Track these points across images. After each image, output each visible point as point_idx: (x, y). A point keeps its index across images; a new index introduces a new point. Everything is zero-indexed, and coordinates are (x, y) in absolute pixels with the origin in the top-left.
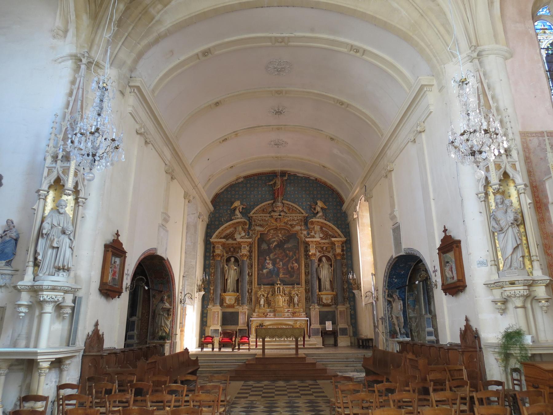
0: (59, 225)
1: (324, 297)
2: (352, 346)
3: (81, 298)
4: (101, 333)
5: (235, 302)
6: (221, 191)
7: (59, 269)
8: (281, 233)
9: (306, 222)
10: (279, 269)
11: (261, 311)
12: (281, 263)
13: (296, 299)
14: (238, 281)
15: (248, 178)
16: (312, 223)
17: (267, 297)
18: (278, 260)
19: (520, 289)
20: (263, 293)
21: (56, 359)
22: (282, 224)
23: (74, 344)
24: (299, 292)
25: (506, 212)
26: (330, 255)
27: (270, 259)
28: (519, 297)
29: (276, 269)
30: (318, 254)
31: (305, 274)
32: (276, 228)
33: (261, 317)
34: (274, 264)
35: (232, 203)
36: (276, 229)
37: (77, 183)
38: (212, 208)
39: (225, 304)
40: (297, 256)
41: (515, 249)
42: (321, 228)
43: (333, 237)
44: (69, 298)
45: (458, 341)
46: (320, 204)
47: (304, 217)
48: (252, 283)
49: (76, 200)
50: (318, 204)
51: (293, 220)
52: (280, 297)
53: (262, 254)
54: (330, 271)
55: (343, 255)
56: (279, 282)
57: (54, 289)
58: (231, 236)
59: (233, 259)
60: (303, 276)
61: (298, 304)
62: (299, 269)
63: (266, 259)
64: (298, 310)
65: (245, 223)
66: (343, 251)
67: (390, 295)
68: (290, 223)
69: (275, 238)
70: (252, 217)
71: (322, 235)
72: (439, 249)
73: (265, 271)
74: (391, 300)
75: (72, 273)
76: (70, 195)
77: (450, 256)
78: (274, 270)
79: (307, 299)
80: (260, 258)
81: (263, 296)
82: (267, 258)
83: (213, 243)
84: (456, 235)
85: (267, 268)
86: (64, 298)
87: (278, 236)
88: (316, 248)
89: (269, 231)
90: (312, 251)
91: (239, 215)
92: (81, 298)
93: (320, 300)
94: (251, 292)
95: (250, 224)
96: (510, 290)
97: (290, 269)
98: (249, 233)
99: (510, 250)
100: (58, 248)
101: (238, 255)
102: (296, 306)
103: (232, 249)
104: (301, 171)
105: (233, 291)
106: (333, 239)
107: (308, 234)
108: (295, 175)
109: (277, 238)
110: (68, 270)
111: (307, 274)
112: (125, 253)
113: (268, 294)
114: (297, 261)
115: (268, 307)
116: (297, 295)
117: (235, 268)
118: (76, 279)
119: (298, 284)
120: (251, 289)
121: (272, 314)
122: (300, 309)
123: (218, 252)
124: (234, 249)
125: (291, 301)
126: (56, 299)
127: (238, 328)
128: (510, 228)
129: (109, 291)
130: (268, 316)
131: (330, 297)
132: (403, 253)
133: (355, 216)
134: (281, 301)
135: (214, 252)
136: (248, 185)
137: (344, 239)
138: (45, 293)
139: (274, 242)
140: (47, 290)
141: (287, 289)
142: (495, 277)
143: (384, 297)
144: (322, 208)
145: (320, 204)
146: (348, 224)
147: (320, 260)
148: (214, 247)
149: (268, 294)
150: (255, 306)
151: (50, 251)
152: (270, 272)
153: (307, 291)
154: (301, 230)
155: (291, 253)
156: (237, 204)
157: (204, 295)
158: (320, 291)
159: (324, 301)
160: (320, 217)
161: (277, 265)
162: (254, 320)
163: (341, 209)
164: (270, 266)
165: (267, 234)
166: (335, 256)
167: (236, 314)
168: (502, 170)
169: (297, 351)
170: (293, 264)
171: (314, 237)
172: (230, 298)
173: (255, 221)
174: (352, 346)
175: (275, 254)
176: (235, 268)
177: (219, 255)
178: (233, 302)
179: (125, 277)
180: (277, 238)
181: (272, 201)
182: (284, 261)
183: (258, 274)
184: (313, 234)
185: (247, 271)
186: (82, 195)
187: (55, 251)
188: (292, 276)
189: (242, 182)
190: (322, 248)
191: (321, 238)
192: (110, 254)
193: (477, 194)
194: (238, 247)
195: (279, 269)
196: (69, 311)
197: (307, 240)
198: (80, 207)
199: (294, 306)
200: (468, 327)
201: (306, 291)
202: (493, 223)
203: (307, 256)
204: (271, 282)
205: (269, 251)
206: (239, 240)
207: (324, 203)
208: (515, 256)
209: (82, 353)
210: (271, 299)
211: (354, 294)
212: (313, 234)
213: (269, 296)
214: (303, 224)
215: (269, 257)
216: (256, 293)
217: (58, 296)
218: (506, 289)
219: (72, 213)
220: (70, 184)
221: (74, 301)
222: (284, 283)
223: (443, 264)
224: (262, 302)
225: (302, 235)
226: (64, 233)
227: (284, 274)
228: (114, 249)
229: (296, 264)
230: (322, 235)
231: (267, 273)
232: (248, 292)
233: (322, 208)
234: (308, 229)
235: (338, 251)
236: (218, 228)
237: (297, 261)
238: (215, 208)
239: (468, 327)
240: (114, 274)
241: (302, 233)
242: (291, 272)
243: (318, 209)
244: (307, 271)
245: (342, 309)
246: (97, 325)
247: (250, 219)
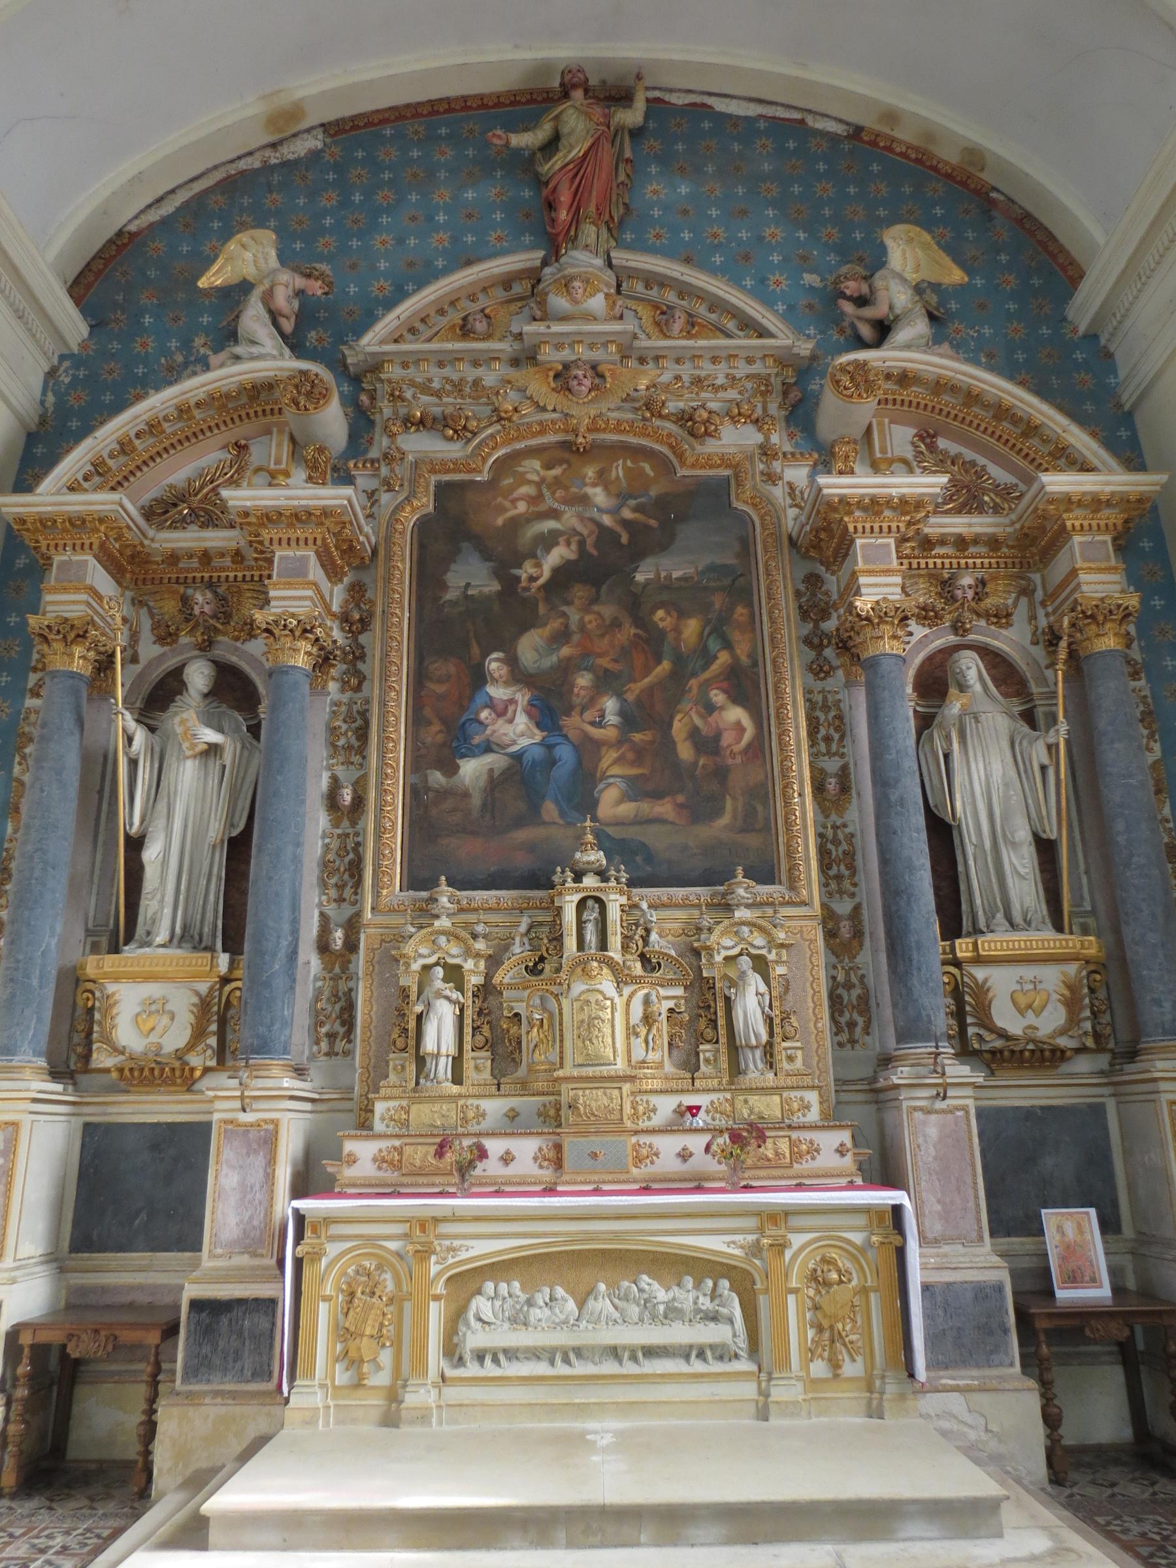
1: (1000, 983)
5: (199, 1034)
6: (153, 216)
8: (602, 478)
9: (796, 399)
10: (588, 749)
11: (423, 1114)
12: (610, 705)
13: (750, 1008)
17: (486, 990)
18: (583, 680)
20: (453, 952)
22: (610, 409)
24: (773, 949)
26: (1012, 640)
27: (518, 675)
29: (565, 753)
31: (819, 788)
32: (566, 446)
36: (569, 451)
38: (74, 326)
39: (102, 1059)
40: (742, 650)
47: (783, 360)
48: (355, 869)
52: (607, 985)
53: (454, 642)
54: (1039, 754)
56: (596, 857)
60: (805, 807)
61: (769, 1050)
62: (758, 750)
63: (479, 678)
64: (769, 1106)
68: (672, 406)
69: (554, 514)
70: (375, 366)
73: (471, 769)
78: (552, 762)
79: (848, 1008)
81: (454, 974)
82: (495, 665)
85: (488, 748)
87: (584, 500)
89: (505, 465)
90: (878, 587)
93: (967, 1004)
94: (351, 946)
97: (685, 752)
102: (753, 1062)
103: (202, 600)
105: (188, 937)
109: (570, 518)
111: (833, 791)
113: (494, 962)
114: (745, 685)
115: (498, 1074)
116: (761, 965)
117: (210, 736)
119: (764, 874)
120: (353, 926)
121: (526, 1148)
122: (795, 1092)
125: (703, 1023)
127: (191, 1291)
130: (491, 1167)
131: (1052, 977)
134: (614, 1018)
139: (549, 541)
141: (668, 916)
147: (935, 683)
149: (494, 962)
150: (376, 1075)
152: (520, 779)
153: (841, 937)
154: (767, 451)
155: (692, 628)
159: (1007, 1019)
161: (574, 723)
162: (329, 1220)
164: (519, 731)
165: (492, 484)
167: (185, 1148)
170: (710, 708)
172: (147, 1005)
175: (562, 637)
176: (210, 736)
178: (175, 1037)
182: (635, 690)
183: (416, 794)
185: (316, 771)
188: (702, 808)
189: (315, 156)
190: (946, 586)
194: (249, 574)
195: (588, 749)
199: (736, 1070)
201: (831, 935)
203: (837, 644)
204: (523, 862)
205: (510, 612)
210: (519, 1002)
213: (503, 976)
215: (512, 661)
216: (390, 958)
222: (646, 869)
224: (440, 1032)
225: (778, 493)
227: (636, 790)
229: (736, 714)
231: (495, 783)
232: (323, 947)
237: (745, 685)
238: (97, 325)
241: (771, 478)
242: (700, 781)
243: (895, 295)
244: (832, 765)
247: (359, 383)
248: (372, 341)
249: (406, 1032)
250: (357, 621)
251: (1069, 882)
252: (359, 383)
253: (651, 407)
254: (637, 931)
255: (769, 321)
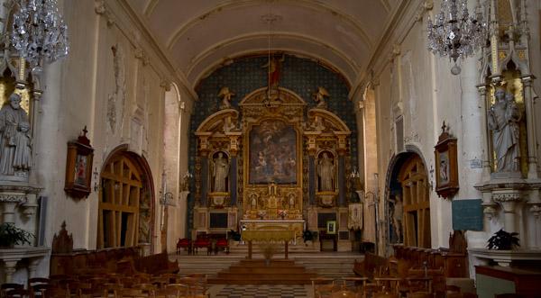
0: (14, 122)
1: (324, 198)
2: (354, 251)
3: (46, 198)
4: (69, 234)
7: (17, 168)
9: (305, 113)
14: (227, 179)
15: (240, 61)
16: (312, 113)
19: (510, 193)
21: (23, 259)
23: (42, 244)
25: (505, 108)
27: (263, 155)
28: (509, 201)
30: (318, 149)
33: (253, 219)
34: (268, 162)
35: (220, 90)
37: (30, 75)
38: (196, 96)
41: (510, 150)
42: (323, 120)
43: (337, 130)
44: (32, 200)
45: (448, 247)
46: (322, 91)
49: (31, 94)
50: (320, 91)
51: (291, 110)
55: (348, 150)
57: (14, 189)
58: (219, 129)
59: (221, 155)
63: (258, 155)
65: (234, 114)
66: (347, 145)
67: (392, 197)
71: (323, 128)
72: (436, 147)
74: (393, 201)
75: (33, 172)
76: (23, 88)
77: (446, 155)
80: (252, 154)
83: (198, 137)
84: (455, 131)
86: (26, 198)
88: (317, 142)
90: (312, 146)
91: (227, 104)
92: (46, 198)
95: (241, 115)
96: (499, 193)
98: (239, 125)
99: (504, 151)
100: (15, 146)
101: (228, 150)
104: (300, 52)
106: (336, 133)
107: (308, 126)
108: (293, 57)
110: (28, 169)
112: (91, 151)
118: (38, 177)
123: (204, 146)
124: (223, 144)
126: (18, 200)
128: (507, 127)
129: (76, 192)
131: (331, 197)
132: (405, 151)
133: (361, 106)
135: (199, 147)
136: (238, 69)
137: (349, 132)
138: (5, 193)
140: (7, 190)
142: (488, 179)
143: (385, 198)
144: (324, 96)
145: (322, 91)
146: (355, 115)
147: (321, 156)
148: (199, 142)
151: (7, 149)
154: (300, 121)
156: (225, 91)
157: (189, 195)
158: (319, 191)
160: (322, 107)
163: (347, 98)
166: (338, 151)
168: (507, 59)
169: (286, 256)
171: (313, 130)
173: (246, 111)
174: (354, 251)
177: (205, 150)
178: (330, 203)
179: (93, 176)
180: (271, 131)
181: (266, 88)
184: (313, 126)
186: (37, 87)
187: (12, 149)
191: (323, 131)
192: (75, 152)
193: (478, 87)
194: (225, 143)
196: (33, 211)
197: (306, 133)
198: (36, 102)
200: (64, 232)
202: (490, 120)
205: (263, 145)
206: (228, 133)
207: (327, 90)
208: (509, 157)
209: (50, 254)
211: (357, 194)
212: (313, 126)
214: (302, 114)
217: (19, 196)
218: (496, 192)
219: (28, 107)
220: (22, 76)
221: (39, 201)
223: (439, 163)
226: (19, 130)
228: (80, 147)
230: (323, 128)
233: (324, 96)
234: (306, 119)
235: (342, 146)
236: (204, 119)
239: (64, 232)
240: (81, 173)
245: (344, 212)
246: (64, 225)
247: (239, 109)
248: (241, 104)
249: (249, 201)
250: (241, 146)
251: (91, 75)
252: (239, 109)
253: (283, 114)
254: (278, 191)
255: (302, 100)
